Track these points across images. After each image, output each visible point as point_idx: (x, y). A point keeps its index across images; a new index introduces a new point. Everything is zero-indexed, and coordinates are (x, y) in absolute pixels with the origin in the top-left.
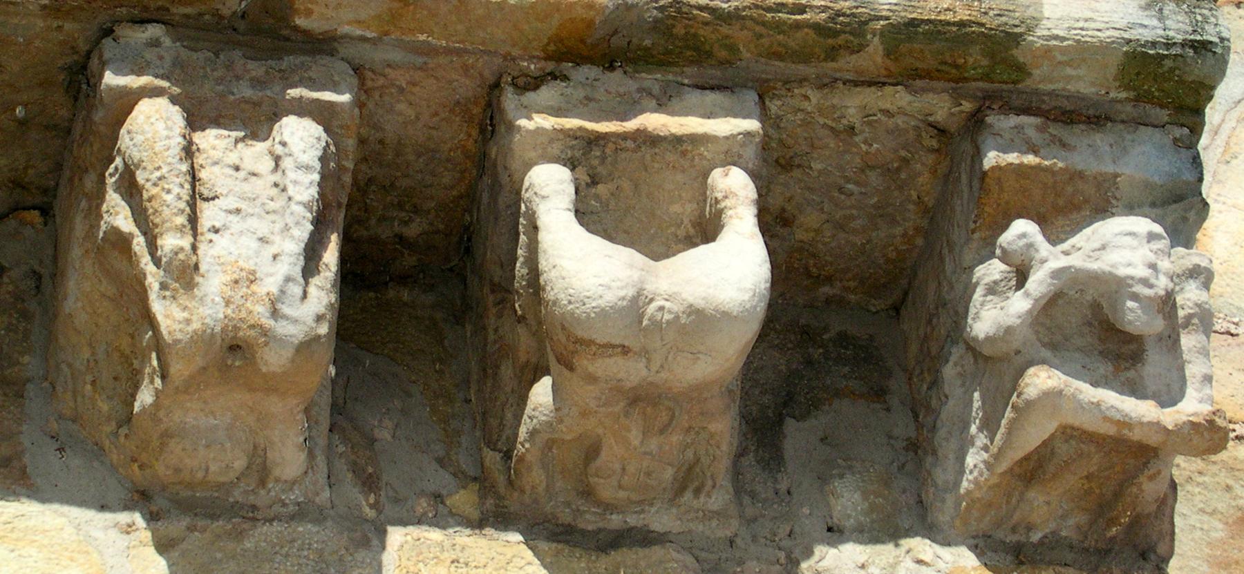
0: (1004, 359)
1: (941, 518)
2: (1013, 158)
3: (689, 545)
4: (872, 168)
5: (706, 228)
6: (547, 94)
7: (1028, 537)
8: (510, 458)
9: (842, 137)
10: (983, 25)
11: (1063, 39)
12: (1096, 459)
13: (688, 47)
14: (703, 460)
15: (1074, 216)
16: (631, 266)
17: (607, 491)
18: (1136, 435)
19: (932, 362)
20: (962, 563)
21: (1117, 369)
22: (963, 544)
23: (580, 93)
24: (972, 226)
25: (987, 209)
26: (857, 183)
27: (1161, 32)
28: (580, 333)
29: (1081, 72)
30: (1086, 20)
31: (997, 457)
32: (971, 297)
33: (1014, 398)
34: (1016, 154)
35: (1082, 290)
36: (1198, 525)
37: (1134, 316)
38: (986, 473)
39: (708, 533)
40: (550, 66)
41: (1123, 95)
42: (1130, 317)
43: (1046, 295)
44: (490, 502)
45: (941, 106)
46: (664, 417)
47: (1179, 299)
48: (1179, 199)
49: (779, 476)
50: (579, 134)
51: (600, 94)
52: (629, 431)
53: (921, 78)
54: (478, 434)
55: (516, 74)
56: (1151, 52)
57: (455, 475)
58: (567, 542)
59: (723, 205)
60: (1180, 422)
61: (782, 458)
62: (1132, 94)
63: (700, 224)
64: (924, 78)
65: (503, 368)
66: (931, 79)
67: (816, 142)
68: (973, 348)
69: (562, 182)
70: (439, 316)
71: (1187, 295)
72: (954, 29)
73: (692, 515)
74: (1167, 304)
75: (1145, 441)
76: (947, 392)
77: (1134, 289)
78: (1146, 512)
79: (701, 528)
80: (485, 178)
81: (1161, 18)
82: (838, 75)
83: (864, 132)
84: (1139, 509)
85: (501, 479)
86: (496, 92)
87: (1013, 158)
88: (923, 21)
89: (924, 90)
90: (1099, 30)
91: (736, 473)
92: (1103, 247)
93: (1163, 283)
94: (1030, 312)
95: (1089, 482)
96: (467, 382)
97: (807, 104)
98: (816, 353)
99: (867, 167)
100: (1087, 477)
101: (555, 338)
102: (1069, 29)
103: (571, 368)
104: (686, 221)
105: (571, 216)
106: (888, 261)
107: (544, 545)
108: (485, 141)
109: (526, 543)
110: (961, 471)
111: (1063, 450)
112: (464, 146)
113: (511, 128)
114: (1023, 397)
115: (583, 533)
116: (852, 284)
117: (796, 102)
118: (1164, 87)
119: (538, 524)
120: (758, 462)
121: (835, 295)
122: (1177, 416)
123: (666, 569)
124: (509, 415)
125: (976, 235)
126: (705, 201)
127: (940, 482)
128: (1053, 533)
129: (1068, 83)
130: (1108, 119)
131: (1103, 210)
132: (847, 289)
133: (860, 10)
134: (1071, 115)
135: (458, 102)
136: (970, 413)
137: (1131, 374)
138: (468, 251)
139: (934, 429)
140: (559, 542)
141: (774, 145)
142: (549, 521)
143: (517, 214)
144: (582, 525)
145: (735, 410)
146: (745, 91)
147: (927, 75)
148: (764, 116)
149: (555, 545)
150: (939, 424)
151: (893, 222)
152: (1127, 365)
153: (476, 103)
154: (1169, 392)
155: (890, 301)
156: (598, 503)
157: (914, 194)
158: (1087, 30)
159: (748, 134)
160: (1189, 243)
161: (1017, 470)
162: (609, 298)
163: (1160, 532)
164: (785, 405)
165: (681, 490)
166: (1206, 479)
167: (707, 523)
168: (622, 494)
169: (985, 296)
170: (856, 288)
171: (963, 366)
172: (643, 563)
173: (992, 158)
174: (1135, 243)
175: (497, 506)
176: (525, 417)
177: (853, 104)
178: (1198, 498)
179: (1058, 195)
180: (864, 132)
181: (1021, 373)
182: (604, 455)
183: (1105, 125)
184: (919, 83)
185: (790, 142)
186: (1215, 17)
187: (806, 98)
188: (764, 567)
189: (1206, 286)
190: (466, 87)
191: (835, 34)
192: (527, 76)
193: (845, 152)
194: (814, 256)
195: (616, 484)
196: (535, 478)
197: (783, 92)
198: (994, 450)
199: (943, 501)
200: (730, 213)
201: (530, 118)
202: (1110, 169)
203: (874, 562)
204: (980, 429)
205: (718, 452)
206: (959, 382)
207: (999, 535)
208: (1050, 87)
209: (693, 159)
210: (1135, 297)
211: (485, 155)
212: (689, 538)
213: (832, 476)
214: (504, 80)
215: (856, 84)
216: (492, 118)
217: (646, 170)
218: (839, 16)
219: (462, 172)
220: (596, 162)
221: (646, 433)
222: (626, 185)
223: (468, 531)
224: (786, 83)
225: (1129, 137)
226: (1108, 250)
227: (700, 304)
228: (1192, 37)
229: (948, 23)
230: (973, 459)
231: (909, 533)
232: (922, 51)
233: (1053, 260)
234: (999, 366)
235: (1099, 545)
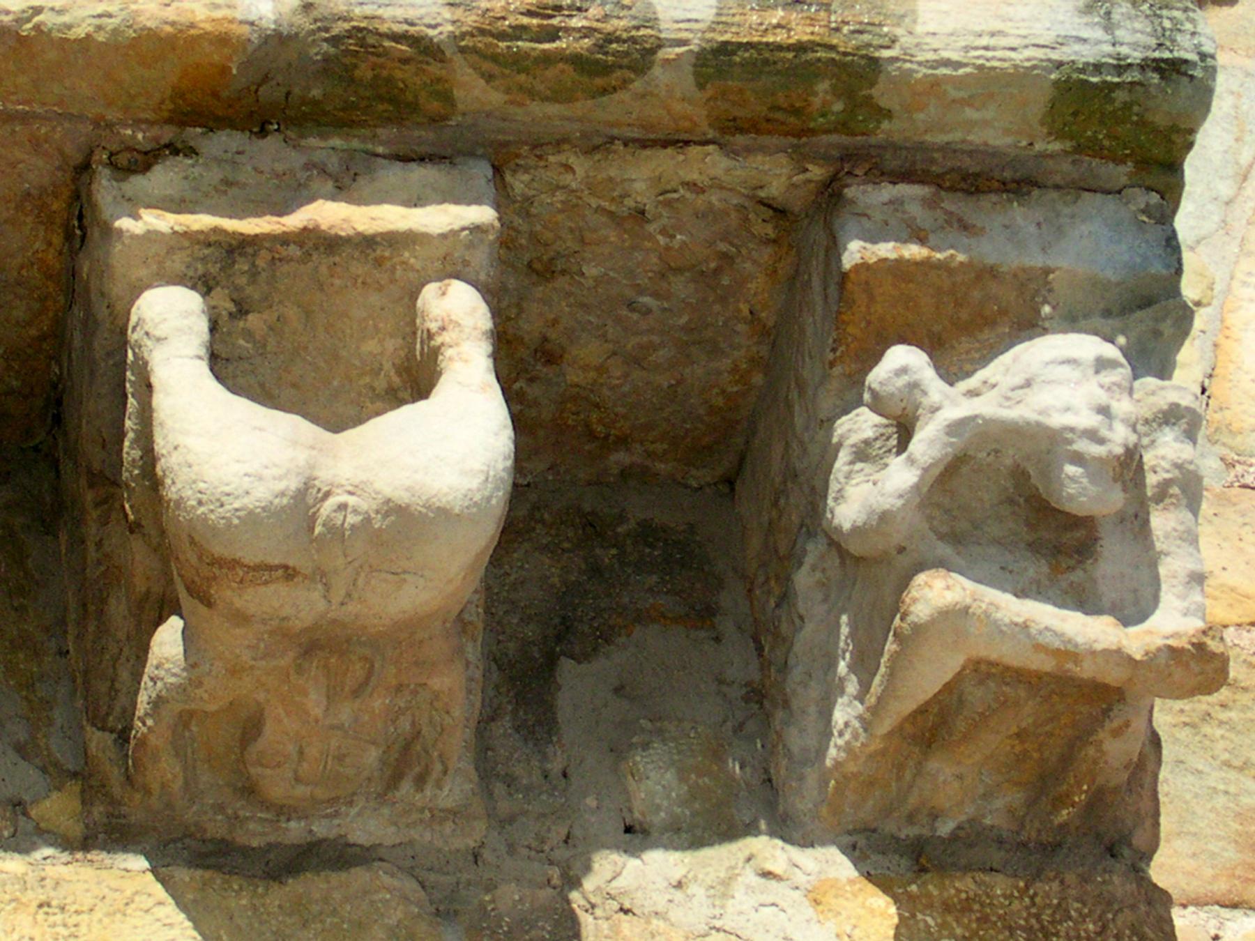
0: (881, 560)
1: (800, 806)
2: (886, 250)
3: (410, 863)
4: (678, 271)
5: (416, 378)
6: (163, 177)
7: (933, 829)
8: (127, 740)
9: (627, 226)
10: (832, 48)
11: (958, 65)
12: (1029, 707)
13: (381, 99)
14: (425, 731)
15: (986, 334)
16: (295, 443)
17: (277, 787)
18: (1086, 671)
19: (782, 562)
20: (832, 873)
21: (1056, 570)
22: (833, 843)
23: (214, 175)
24: (831, 356)
25: (850, 329)
26: (656, 295)
27: (1107, 48)
28: (218, 550)
29: (989, 114)
30: (993, 34)
31: (875, 710)
32: (831, 466)
33: (897, 621)
34: (891, 245)
35: (997, 451)
36: (1221, 787)
37: (1077, 487)
38: (863, 737)
39: (439, 843)
40: (168, 134)
41: (1056, 146)
42: (1071, 489)
43: (941, 460)
44: (98, 811)
45: (776, 174)
46: (359, 670)
47: (1148, 458)
48: (1146, 302)
49: (550, 750)
50: (213, 238)
51: (246, 175)
52: (306, 694)
53: (741, 130)
54: (80, 703)
55: (114, 147)
56: (1094, 80)
57: (44, 770)
58: (218, 868)
59: (438, 340)
60: (1153, 648)
61: (554, 720)
62: (1068, 145)
63: (408, 370)
64: (747, 131)
65: (112, 601)
66: (758, 132)
67: (589, 236)
68: (835, 542)
69: (187, 314)
70: (18, 521)
71: (1161, 451)
72: (790, 55)
73: (415, 816)
74: (1129, 466)
75: (1100, 678)
76: (802, 612)
77: (1075, 447)
78: (1112, 784)
79: (428, 836)
80: (75, 309)
81: (1109, 27)
82: (615, 132)
83: (661, 216)
84: (1100, 780)
85: (115, 775)
86: (85, 178)
87: (886, 250)
88: (740, 45)
89: (749, 150)
90: (1013, 49)
91: (483, 749)
92: (1028, 384)
93: (1120, 437)
94: (916, 487)
95: (1022, 742)
96: (63, 622)
97: (569, 177)
98: (607, 556)
99: (668, 270)
100: (1018, 735)
101: (182, 557)
102: (967, 49)
103: (209, 604)
104: (387, 366)
105: (203, 367)
106: (712, 410)
107: (183, 874)
108: (74, 254)
109: (154, 870)
110: (826, 733)
111: (977, 696)
112: (40, 260)
113: (108, 232)
114: (910, 619)
115: (246, 851)
116: (660, 447)
117: (551, 175)
118: (1119, 132)
119: (174, 841)
120: (517, 730)
121: (632, 465)
122: (1148, 639)
123: (372, 902)
124: (124, 675)
125: (837, 370)
126: (414, 333)
127: (795, 749)
128: (971, 821)
129: (969, 132)
130: (1036, 185)
131: (1028, 326)
132: (650, 455)
133: (642, 32)
134: (973, 181)
135: (29, 194)
136: (837, 643)
137: (1077, 576)
138: (58, 420)
139: (785, 668)
140: (208, 867)
141: (523, 242)
142: (191, 836)
143: (122, 365)
144: (241, 838)
145: (473, 652)
146: (471, 162)
147: (753, 127)
148: (502, 199)
149: (199, 872)
150: (791, 662)
151: (715, 351)
152: (1072, 562)
153: (56, 195)
154: (1136, 602)
155: (720, 471)
156: (266, 805)
157: (745, 308)
158: (994, 49)
159: (476, 229)
160: (1164, 371)
161: (909, 728)
162: (261, 494)
163: (1137, 813)
164: (559, 638)
165: (394, 781)
166: (1233, 715)
167: (437, 828)
168: (301, 791)
169: (852, 463)
170: (665, 452)
171: (824, 570)
172: (337, 895)
173: (855, 252)
174: (1076, 374)
175: (109, 815)
176: (145, 678)
177: (641, 176)
178: (1221, 744)
179: (958, 304)
180: (661, 216)
181: (904, 582)
182: (269, 729)
183: (1029, 193)
184: (740, 140)
185: (548, 235)
186: (1192, 21)
187: (568, 168)
188: (527, 892)
189: (1191, 435)
190: (38, 171)
191: (606, 69)
192: (131, 149)
193: (634, 248)
194: (597, 406)
195: (290, 775)
196: (166, 770)
197: (532, 161)
198: (871, 700)
199: (801, 778)
200: (449, 352)
201: (137, 217)
202: (1036, 260)
203: (695, 879)
204: (852, 668)
205: (448, 720)
206: (819, 596)
207: (890, 827)
208: (941, 138)
209: (394, 268)
210: (1078, 459)
211: (74, 274)
212: (410, 852)
213: (631, 746)
214: (96, 158)
215: (644, 144)
216: (81, 217)
217: (322, 290)
218: (611, 42)
219: (43, 299)
220: (242, 281)
221: (332, 697)
222: (292, 312)
223: (66, 856)
224: (534, 147)
225: (1067, 211)
226: (1035, 387)
227: (402, 497)
228: (1157, 55)
229: (779, 47)
230: (844, 713)
231: (750, 830)
232: (741, 91)
233: (949, 406)
234: (873, 571)
235: (1044, 837)
